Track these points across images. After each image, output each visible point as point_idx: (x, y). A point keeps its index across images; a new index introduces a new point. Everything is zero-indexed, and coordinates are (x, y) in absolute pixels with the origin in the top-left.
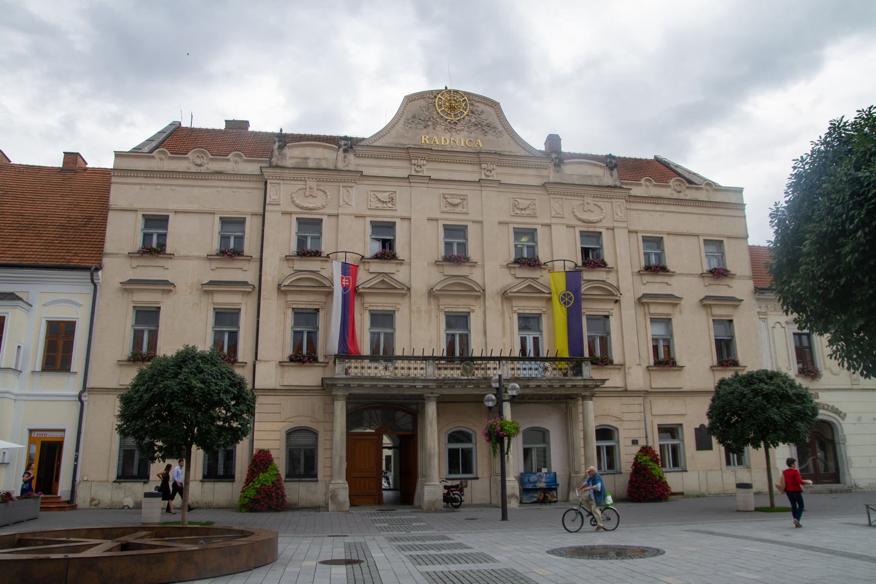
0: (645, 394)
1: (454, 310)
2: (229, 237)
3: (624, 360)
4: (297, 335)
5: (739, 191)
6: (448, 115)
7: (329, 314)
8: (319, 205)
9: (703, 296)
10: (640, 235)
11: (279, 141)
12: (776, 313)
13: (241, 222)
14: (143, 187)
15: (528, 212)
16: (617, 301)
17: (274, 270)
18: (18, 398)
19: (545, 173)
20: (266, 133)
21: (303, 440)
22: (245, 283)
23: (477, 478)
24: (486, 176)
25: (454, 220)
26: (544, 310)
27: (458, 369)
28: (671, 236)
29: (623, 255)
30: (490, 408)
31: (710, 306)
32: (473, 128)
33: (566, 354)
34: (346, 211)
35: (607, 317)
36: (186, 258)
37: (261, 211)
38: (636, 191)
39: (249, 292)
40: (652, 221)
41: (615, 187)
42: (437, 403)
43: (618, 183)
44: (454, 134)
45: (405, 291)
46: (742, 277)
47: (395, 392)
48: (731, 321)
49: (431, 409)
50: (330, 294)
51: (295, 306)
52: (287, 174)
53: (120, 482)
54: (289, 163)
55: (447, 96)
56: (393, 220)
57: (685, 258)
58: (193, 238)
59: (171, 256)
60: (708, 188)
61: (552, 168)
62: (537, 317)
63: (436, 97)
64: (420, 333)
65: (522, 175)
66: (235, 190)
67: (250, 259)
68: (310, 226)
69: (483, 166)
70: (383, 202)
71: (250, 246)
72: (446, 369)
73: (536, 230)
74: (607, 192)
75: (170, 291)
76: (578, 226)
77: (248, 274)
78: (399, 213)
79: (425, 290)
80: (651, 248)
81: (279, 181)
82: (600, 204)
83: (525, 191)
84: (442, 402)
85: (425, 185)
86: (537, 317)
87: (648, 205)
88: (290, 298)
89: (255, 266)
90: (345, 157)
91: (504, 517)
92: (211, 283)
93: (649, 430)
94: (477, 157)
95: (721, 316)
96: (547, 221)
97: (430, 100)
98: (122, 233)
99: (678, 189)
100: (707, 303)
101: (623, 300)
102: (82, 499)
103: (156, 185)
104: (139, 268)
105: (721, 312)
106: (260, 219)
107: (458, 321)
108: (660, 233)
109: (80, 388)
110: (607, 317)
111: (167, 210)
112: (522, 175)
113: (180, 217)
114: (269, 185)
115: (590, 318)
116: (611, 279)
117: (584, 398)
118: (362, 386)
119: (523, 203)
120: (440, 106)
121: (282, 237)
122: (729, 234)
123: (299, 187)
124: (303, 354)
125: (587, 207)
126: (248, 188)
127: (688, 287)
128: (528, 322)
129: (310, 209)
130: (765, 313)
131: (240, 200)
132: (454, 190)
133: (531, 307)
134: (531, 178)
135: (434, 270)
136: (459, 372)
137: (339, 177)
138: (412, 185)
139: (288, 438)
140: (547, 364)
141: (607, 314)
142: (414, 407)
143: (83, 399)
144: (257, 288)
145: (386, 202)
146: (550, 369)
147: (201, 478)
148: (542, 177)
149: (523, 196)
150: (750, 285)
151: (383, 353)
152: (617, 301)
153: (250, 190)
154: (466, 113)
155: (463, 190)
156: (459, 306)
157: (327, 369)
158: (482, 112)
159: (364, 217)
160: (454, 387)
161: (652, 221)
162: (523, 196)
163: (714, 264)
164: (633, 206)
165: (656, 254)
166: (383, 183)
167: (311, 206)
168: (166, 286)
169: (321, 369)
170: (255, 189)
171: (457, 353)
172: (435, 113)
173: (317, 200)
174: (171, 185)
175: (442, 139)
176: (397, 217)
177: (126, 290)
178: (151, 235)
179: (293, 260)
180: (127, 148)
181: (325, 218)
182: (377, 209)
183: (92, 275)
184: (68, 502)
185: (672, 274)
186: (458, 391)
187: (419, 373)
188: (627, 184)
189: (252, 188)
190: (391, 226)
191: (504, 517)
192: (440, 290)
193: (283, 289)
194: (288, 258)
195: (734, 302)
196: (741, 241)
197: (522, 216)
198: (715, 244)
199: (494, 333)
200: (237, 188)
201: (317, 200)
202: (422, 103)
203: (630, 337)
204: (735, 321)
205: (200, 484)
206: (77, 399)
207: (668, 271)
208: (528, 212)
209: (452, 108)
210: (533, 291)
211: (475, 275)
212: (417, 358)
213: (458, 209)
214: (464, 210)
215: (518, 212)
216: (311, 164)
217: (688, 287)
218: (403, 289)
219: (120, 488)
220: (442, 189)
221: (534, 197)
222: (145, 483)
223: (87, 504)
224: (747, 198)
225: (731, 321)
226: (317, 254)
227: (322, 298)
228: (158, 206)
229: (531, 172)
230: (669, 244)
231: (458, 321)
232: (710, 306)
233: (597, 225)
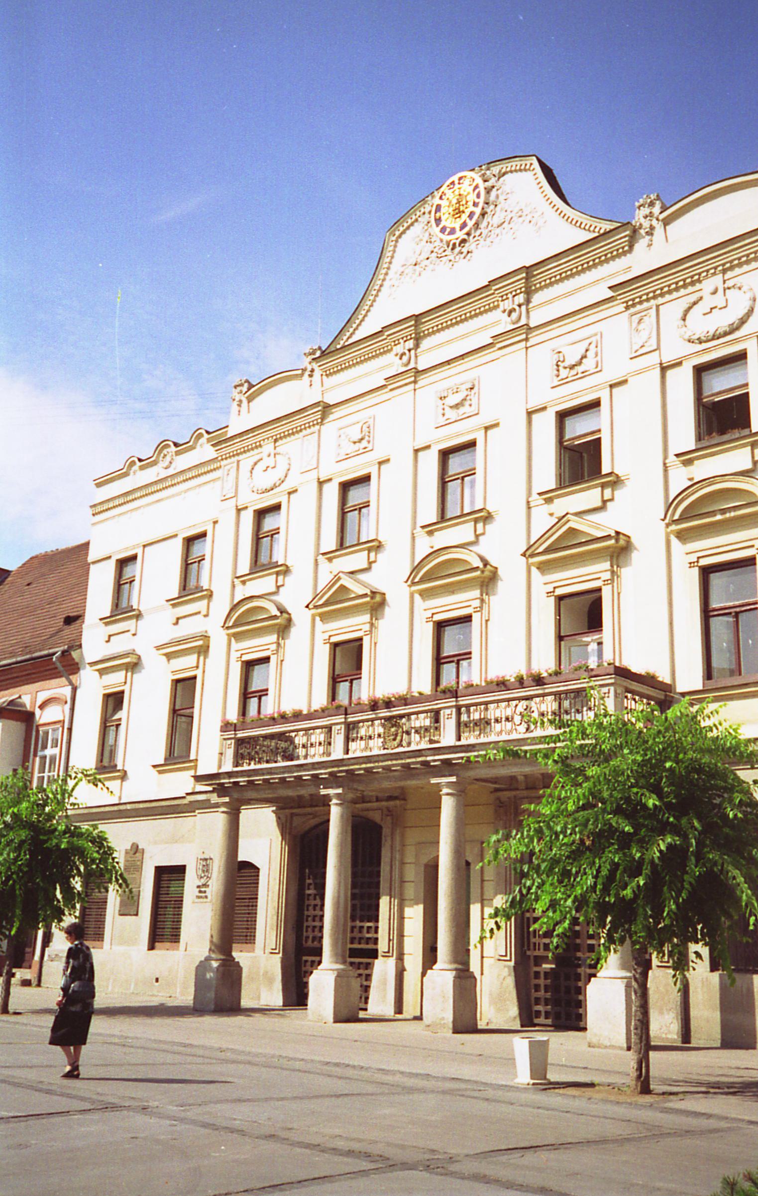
52: (238, 445)
213: (466, 410)
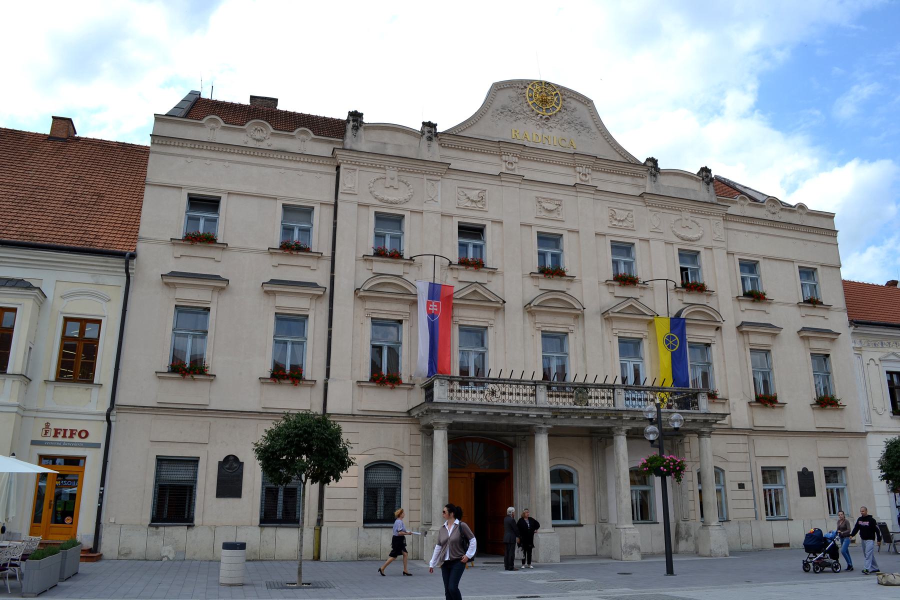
0: (751, 432)
1: (552, 329)
2: (383, 236)
4: (377, 350)
5: (831, 216)
7: (414, 326)
8: (402, 198)
9: (800, 328)
10: (737, 257)
11: (353, 121)
12: (869, 349)
13: (308, 211)
14: (189, 160)
15: (625, 224)
16: (718, 328)
17: (351, 272)
18: (27, 414)
19: (640, 181)
21: (382, 477)
22: (314, 285)
23: (582, 526)
24: (582, 180)
25: (550, 227)
26: (646, 334)
27: (571, 397)
28: (767, 261)
29: (720, 276)
30: (652, 442)
31: (808, 338)
32: (565, 126)
33: (669, 383)
34: (431, 209)
35: (708, 345)
36: (242, 250)
37: (333, 201)
38: (734, 209)
39: (319, 296)
40: (751, 243)
41: (712, 203)
42: (549, 436)
43: (714, 200)
45: (498, 306)
46: (838, 310)
47: (504, 422)
48: (828, 356)
49: (542, 442)
50: (414, 303)
51: (375, 316)
52: (365, 159)
53: (157, 527)
54: (363, 146)
56: (560, 232)
57: (780, 283)
58: (249, 225)
59: (224, 246)
60: (801, 211)
61: (648, 177)
62: (637, 342)
64: (514, 352)
65: (618, 183)
66: (301, 173)
67: (319, 256)
68: (390, 221)
69: (578, 169)
70: (472, 201)
71: (319, 240)
72: (558, 396)
73: (403, 216)
74: (705, 209)
75: (223, 289)
76: (374, 206)
77: (320, 276)
78: (492, 215)
79: (520, 306)
80: (548, 247)
81: (355, 167)
82: (697, 220)
84: (554, 435)
85: (518, 185)
86: (637, 342)
87: (774, 230)
88: (370, 305)
89: (326, 265)
90: (429, 146)
91: (670, 571)
92: (273, 282)
93: (754, 473)
94: (574, 158)
95: (819, 349)
96: (646, 236)
98: (162, 215)
99: (773, 210)
100: (806, 334)
101: (724, 326)
102: (108, 546)
103: (206, 159)
104: (183, 259)
105: (820, 346)
106: (331, 210)
107: (554, 341)
108: (756, 256)
109: (107, 405)
110: (708, 345)
111: (219, 190)
112: (618, 183)
113: (234, 198)
115: (463, 329)
116: (712, 302)
117: (700, 434)
118: (469, 413)
119: (621, 215)
120: (531, 97)
121: (358, 233)
122: (822, 261)
123: (378, 176)
124: (384, 375)
125: (685, 223)
126: (316, 172)
127: (785, 314)
128: (630, 346)
129: (392, 203)
130: (860, 349)
131: (311, 187)
133: (632, 330)
134: (626, 185)
135: (529, 282)
136: (571, 400)
137: (423, 168)
138: (503, 184)
139: (366, 475)
140: (495, 387)
141: (709, 342)
142: (511, 439)
143: (112, 418)
144: (328, 291)
145: (475, 202)
146: (498, 394)
147: (258, 523)
148: (638, 186)
149: (620, 206)
150: (844, 318)
151: (473, 377)
152: (718, 328)
153: (318, 175)
154: (558, 108)
155: (558, 194)
156: (557, 324)
157: (412, 392)
158: (575, 109)
159: (367, 206)
160: (582, 417)
161: (751, 243)
162: (620, 206)
163: (808, 295)
164: (732, 225)
165: (625, 263)
166: (471, 179)
167: (391, 199)
168: (218, 283)
169: (406, 392)
170: (326, 173)
171: (554, 379)
172: (525, 105)
173: (395, 192)
174: (224, 161)
175: (529, 132)
176: (487, 220)
177: (167, 284)
178: (198, 219)
179: (372, 261)
180: (164, 111)
181: (407, 215)
182: (466, 208)
183: (127, 264)
184: (90, 551)
185: (770, 302)
186: (574, 422)
187: (509, 400)
188: (722, 201)
189: (321, 173)
190: (398, 220)
191: (670, 571)
192: (538, 306)
193: (362, 294)
194: (366, 258)
195: (830, 335)
196: (835, 269)
197: (620, 228)
198: (807, 273)
199: (594, 358)
200: (303, 171)
201: (395, 192)
202: (512, 93)
203: (730, 371)
204: (831, 356)
205: (259, 529)
206: (104, 418)
207: (821, 303)
208: (625, 224)
209: (544, 102)
210: (634, 312)
211: (495, 285)
212: (504, 382)
213: (554, 215)
214: (560, 218)
215: (615, 223)
216: (390, 151)
217: (785, 314)
218: (498, 302)
219: (157, 534)
220: (535, 192)
221: (631, 207)
222: (189, 526)
223: (115, 555)
224: (838, 224)
225: (828, 356)
226: (396, 256)
227: (405, 308)
228: (300, 195)
229: (627, 180)
230: (764, 268)
231: (554, 341)
232: (808, 338)
233: (696, 243)
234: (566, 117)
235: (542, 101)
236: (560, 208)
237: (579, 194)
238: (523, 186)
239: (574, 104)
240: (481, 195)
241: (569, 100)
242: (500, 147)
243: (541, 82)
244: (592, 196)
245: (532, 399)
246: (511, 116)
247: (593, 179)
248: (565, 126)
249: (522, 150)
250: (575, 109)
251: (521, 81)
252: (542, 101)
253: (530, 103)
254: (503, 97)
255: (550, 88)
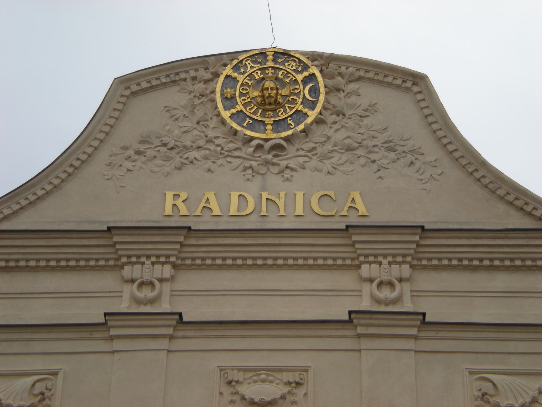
3: (167, 356)
6: (255, 124)
20: (495, 168)
44: (273, 180)
55: (250, 67)
63: (217, 75)
69: (136, 272)
83: (522, 347)
85: (164, 344)
94: (348, 242)
97: (200, 87)
114: (112, 115)
120: (229, 101)
132: (262, 351)
138: (118, 345)
154: (312, 115)
155: (293, 353)
158: (372, 109)
166: (16, 347)
172: (213, 123)
175: (228, 196)
202: (176, 97)
209: (270, 104)
234: (341, 135)
235: (261, 105)
236: (301, 391)
237: (365, 343)
238: (179, 344)
239: (368, 94)
240: (39, 388)
241: (353, 86)
242: (111, 244)
243: (263, 54)
244: (410, 344)
245: (471, 170)
246: (168, 159)
247: (415, 295)
248: (336, 158)
249: (186, 243)
250: (372, 109)
251: (203, 61)
252: (261, 105)
253: (226, 115)
254: (147, 115)
255: (290, 66)
